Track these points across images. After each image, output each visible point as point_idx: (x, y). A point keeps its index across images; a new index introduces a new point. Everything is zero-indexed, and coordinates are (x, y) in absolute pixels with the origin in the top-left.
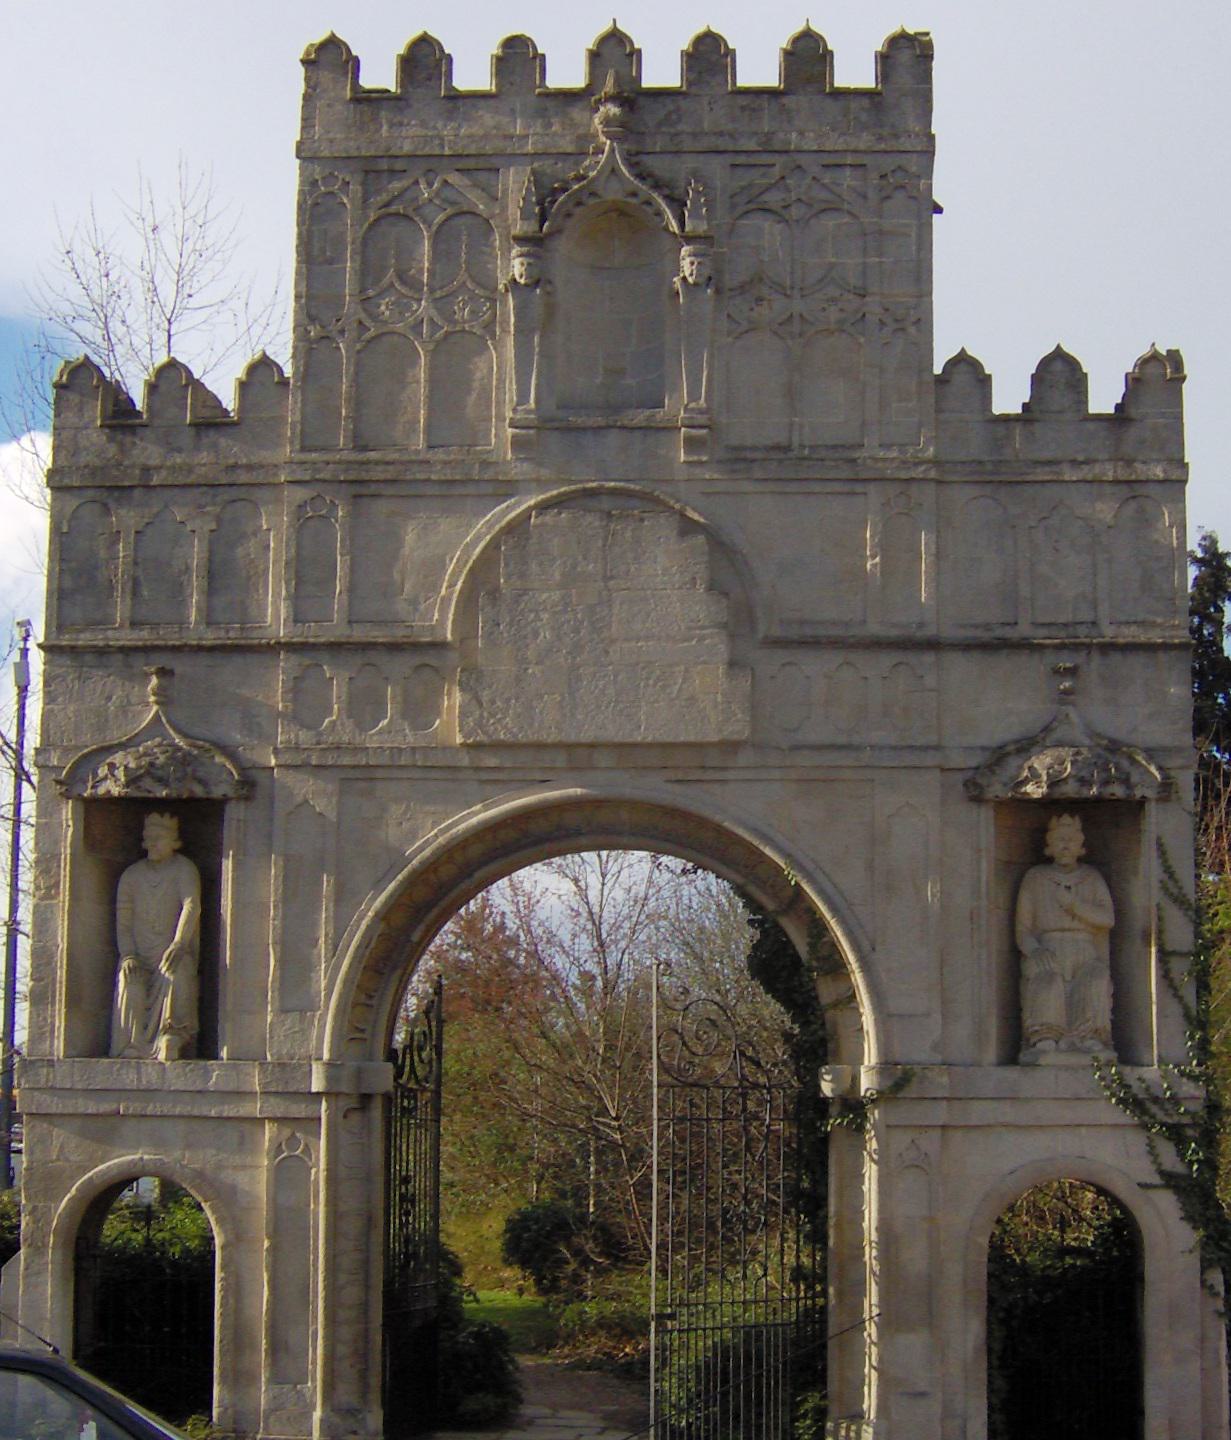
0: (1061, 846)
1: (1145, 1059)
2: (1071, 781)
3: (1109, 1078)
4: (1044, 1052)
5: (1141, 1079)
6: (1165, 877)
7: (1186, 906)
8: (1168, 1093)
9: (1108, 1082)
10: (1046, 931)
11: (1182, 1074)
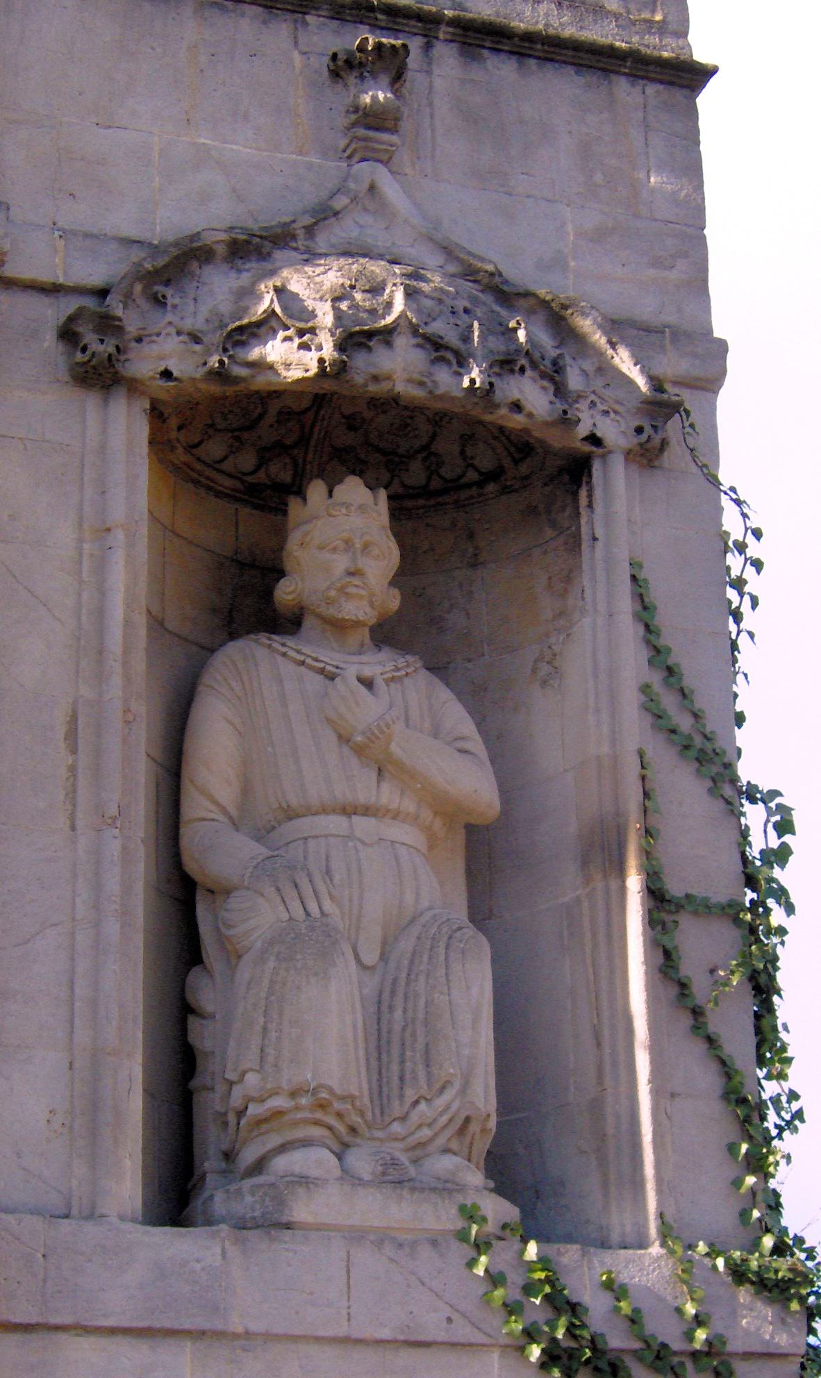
0: (341, 563)
1: (619, 1222)
2: (403, 342)
3: (516, 1278)
4: (304, 1181)
5: (614, 1288)
6: (656, 679)
7: (714, 769)
8: (701, 1335)
9: (517, 1295)
10: (290, 814)
11: (738, 1273)
